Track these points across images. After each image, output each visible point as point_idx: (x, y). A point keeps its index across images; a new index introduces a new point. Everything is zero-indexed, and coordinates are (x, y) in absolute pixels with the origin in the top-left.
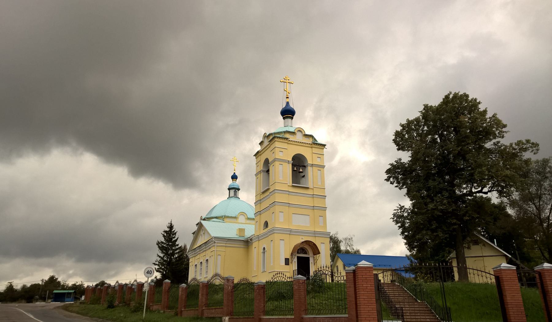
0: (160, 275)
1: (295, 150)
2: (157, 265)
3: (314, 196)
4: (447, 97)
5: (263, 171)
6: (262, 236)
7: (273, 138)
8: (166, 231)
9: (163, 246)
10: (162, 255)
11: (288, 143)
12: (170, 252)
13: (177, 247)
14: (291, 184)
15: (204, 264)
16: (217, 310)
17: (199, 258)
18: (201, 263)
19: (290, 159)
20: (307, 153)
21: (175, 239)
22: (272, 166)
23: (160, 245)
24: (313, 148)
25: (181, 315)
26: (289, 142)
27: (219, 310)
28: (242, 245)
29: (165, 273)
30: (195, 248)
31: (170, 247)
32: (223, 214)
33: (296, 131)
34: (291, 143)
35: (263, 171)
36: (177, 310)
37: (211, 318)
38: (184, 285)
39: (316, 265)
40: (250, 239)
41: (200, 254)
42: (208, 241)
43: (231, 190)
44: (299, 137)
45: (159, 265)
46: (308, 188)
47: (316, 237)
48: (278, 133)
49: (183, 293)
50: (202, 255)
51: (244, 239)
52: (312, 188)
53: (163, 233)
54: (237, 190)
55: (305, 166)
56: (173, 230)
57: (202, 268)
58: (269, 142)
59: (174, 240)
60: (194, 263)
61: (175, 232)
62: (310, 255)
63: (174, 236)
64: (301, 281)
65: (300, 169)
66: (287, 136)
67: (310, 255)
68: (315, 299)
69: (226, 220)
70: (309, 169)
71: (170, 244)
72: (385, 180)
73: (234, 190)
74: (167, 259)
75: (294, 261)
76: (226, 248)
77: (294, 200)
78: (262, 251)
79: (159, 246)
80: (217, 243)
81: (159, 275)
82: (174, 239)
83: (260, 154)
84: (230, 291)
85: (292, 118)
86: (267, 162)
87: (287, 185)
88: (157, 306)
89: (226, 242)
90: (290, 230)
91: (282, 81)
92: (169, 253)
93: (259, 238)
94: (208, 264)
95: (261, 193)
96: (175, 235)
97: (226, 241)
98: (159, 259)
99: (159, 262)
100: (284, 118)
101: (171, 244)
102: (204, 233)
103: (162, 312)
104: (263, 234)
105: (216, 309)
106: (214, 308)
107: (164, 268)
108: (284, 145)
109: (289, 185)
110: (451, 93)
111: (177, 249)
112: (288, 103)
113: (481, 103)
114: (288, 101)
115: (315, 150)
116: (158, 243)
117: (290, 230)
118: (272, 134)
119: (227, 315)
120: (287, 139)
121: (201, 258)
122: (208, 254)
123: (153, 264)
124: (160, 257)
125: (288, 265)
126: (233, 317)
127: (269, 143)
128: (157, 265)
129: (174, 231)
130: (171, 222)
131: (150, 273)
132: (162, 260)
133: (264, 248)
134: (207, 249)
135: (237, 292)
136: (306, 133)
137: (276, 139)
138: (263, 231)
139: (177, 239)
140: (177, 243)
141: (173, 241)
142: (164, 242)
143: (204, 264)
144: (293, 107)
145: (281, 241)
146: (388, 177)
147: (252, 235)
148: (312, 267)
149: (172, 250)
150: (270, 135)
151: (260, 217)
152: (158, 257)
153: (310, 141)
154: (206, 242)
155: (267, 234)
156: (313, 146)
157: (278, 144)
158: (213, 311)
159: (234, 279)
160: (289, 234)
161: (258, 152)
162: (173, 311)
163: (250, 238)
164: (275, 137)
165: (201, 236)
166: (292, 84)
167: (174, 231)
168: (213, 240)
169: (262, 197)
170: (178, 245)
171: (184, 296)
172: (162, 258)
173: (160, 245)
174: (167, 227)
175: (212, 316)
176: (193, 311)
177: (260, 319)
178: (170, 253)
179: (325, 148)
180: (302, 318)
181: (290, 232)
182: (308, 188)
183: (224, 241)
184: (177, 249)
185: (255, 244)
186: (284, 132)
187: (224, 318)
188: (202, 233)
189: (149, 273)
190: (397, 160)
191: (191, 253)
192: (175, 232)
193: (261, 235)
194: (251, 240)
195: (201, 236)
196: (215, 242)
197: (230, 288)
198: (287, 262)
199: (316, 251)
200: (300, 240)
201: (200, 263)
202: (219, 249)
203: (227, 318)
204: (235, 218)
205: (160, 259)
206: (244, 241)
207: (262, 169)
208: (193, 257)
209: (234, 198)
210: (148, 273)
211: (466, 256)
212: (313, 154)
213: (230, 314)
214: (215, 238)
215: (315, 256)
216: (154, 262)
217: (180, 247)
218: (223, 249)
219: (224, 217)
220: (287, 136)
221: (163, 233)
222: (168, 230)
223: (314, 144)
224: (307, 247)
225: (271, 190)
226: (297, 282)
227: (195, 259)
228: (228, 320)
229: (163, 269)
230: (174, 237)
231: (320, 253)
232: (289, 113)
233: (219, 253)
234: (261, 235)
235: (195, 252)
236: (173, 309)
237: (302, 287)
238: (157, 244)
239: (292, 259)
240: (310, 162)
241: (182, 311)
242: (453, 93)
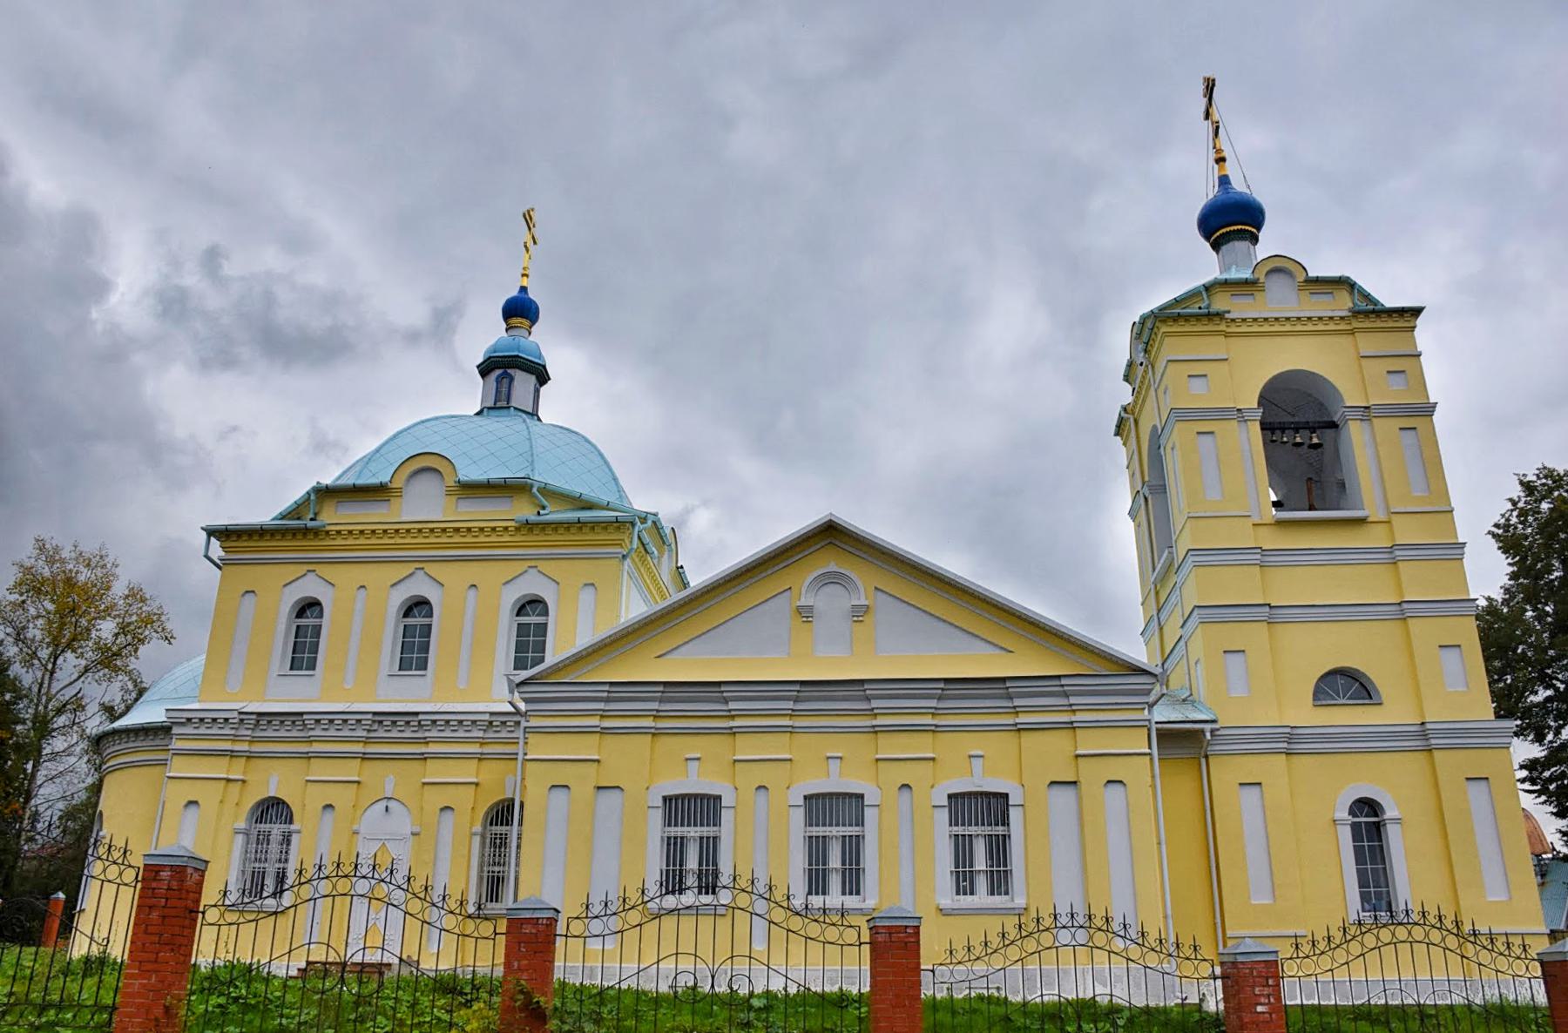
3: (1398, 553)
11: (1227, 335)
26: (1233, 329)
34: (1244, 329)
38: (244, 1030)
46: (1361, 521)
52: (1382, 517)
55: (1333, 425)
70: (1356, 435)
76: (367, 764)
87: (1250, 522)
90: (1288, 730)
100: (1216, 246)
112: (1224, 181)
115: (1370, 343)
120: (1220, 315)
135: (1374, 976)
136: (1312, 274)
144: (1248, 192)
145: (1247, 790)
153: (1342, 303)
160: (1287, 754)
182: (1361, 521)
211: (922, 967)
212: (1364, 361)
220: (1220, 303)
223: (1367, 314)
240: (1352, 397)
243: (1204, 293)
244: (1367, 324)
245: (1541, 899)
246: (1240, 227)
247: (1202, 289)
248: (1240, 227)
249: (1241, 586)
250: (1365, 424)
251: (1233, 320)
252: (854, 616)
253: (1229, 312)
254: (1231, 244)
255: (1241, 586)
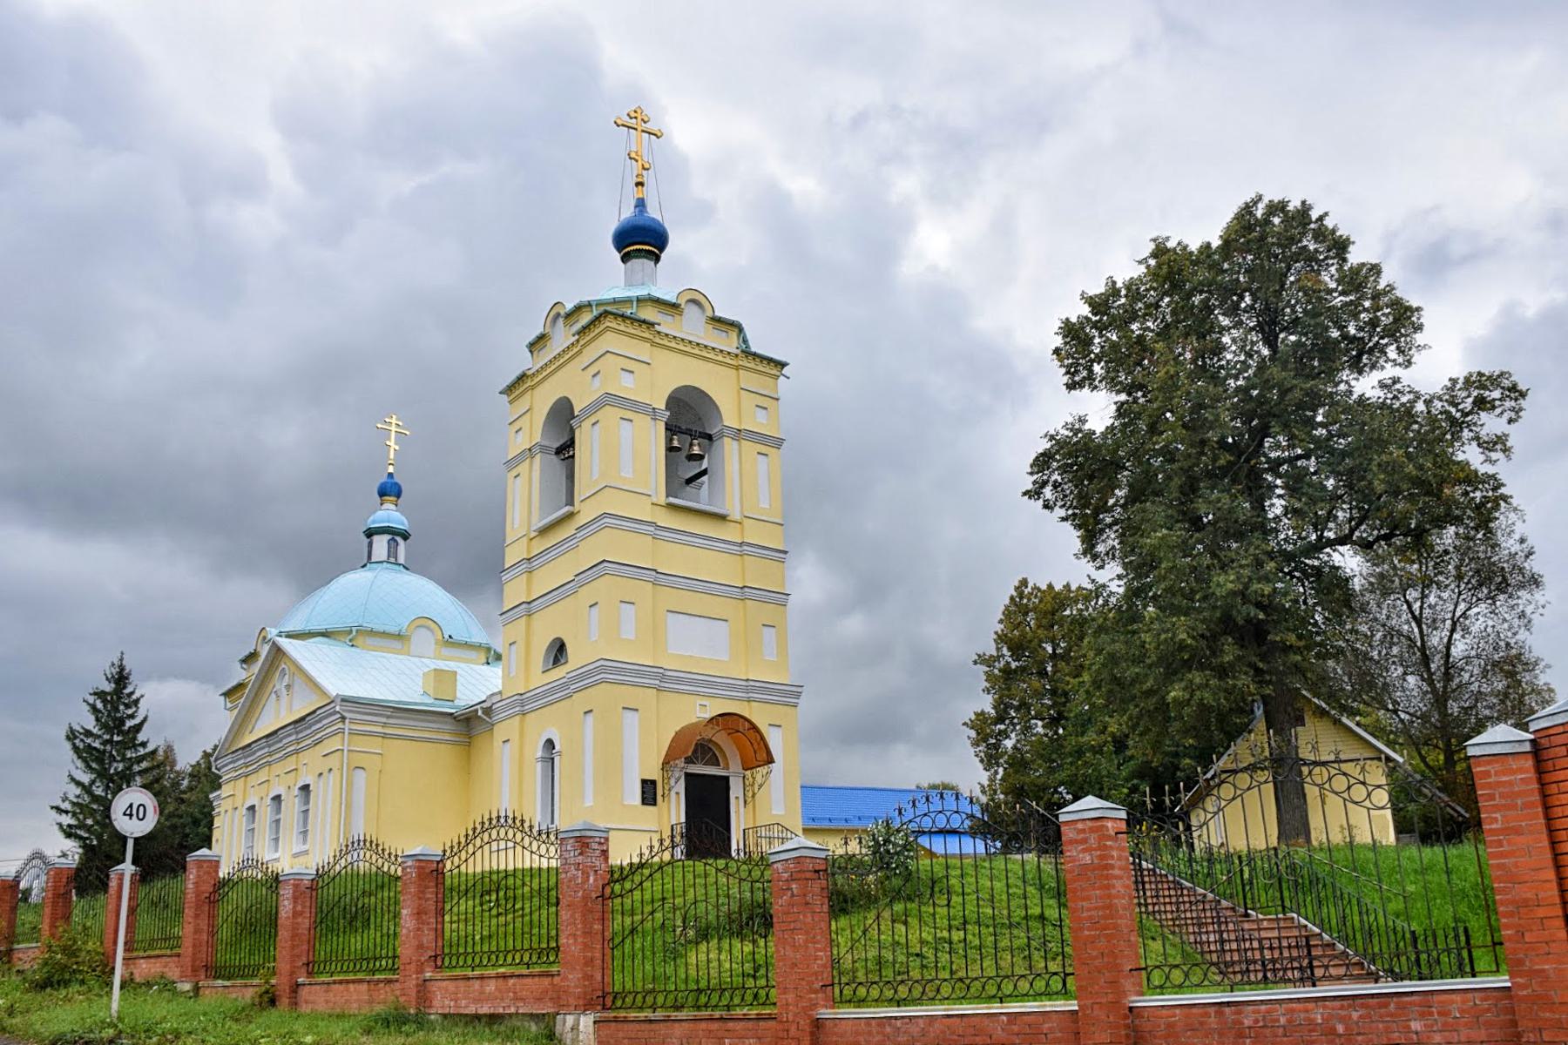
0: (80, 851)
1: (674, 372)
2: (67, 812)
3: (745, 548)
4: (1248, 209)
5: (544, 449)
6: (537, 697)
7: (597, 319)
8: (103, 692)
9: (89, 745)
10: (86, 778)
11: (653, 344)
12: (115, 769)
13: (142, 751)
14: (662, 499)
15: (292, 805)
16: (512, 981)
17: (296, 769)
18: (277, 798)
19: (661, 404)
20: (719, 385)
21: (137, 721)
22: (587, 424)
23: (77, 741)
24: (741, 371)
25: (294, 1004)
26: (657, 340)
27: (529, 980)
28: (446, 731)
29: (95, 842)
30: (249, 745)
31: (117, 751)
32: (350, 622)
33: (682, 301)
34: (665, 342)
35: (544, 449)
36: (273, 981)
37: (477, 1017)
39: (750, 806)
40: (482, 708)
41: (269, 764)
42: (314, 712)
43: (375, 538)
44: (691, 326)
45: (74, 814)
46: (722, 518)
47: (753, 704)
48: (615, 302)
49: (299, 908)
50: (279, 768)
51: (453, 711)
53: (91, 699)
54: (398, 539)
55: (710, 437)
56: (127, 691)
57: (253, 829)
58: (579, 333)
59: (130, 727)
60: (244, 799)
61: (134, 697)
62: (731, 770)
63: (130, 712)
64: (1109, 824)
65: (691, 445)
66: (648, 313)
67: (732, 770)
68: (905, 923)
69: (360, 641)
70: (729, 447)
71: (116, 738)
72: (1025, 494)
73: (389, 537)
74: (103, 794)
75: (673, 793)
76: (386, 741)
77: (675, 559)
78: (539, 754)
79: (74, 744)
80: (352, 721)
81: (74, 850)
82: (129, 723)
83: (529, 383)
84: (594, 895)
85: (657, 259)
86: (563, 415)
87: (648, 501)
88: (153, 960)
89: (384, 720)
90: (661, 671)
91: (619, 122)
92: (112, 771)
93: (523, 704)
94: (307, 802)
95: (533, 534)
96: (136, 706)
97: (388, 717)
98: (74, 791)
99: (74, 804)
100: (626, 258)
101: (120, 738)
102: (288, 687)
103: (187, 987)
104: (546, 687)
105: (504, 977)
106: (491, 972)
107: (92, 826)
108: (642, 351)
109: (655, 500)
110: (1260, 198)
111: (140, 760)
112: (641, 204)
113: (1353, 243)
114: (641, 196)
115: (750, 380)
116: (72, 736)
117: (661, 671)
118: (589, 305)
119: (587, 1007)
121: (279, 779)
122: (309, 765)
123: (52, 808)
124: (78, 783)
125: (655, 804)
126: (612, 1014)
127: (577, 337)
128: (67, 812)
129: (132, 693)
130: (121, 660)
131: (141, 816)
132: (86, 796)
133: (550, 744)
134: (274, 757)
136: (718, 314)
137: (609, 322)
138: (539, 679)
139: (145, 719)
140: (141, 737)
141: (126, 728)
142: (95, 731)
143: (292, 805)
144: (660, 219)
146: (1035, 482)
147: (493, 695)
148: (737, 812)
149: (124, 759)
150: (578, 309)
151: (528, 625)
152: (73, 786)
153: (730, 343)
154: (302, 719)
155: (565, 686)
156: (741, 363)
157: (611, 340)
158: (491, 986)
159: (607, 839)
161: (522, 378)
162: (246, 986)
163: (484, 705)
164: (606, 313)
165: (273, 696)
166: (658, 137)
167: (132, 693)
168: (338, 709)
169: (538, 546)
170: (144, 744)
171: (307, 921)
172: (87, 789)
173: (77, 741)
174: (107, 679)
175: (485, 1009)
176: (364, 987)
177: (818, 1024)
178: (117, 773)
179: (782, 377)
180: (1131, 1009)
181: (662, 680)
182: (722, 518)
183: (376, 715)
184: (140, 760)
185: (505, 729)
186: (639, 300)
187: (570, 1020)
188: (278, 683)
189: (134, 817)
190: (1070, 420)
191: (231, 763)
192: (134, 697)
193: (533, 693)
194: (488, 711)
195: (273, 696)
196: (343, 718)
197: (591, 879)
198: (649, 793)
199: (759, 755)
200: (700, 710)
201: (273, 799)
202: (361, 744)
203: (587, 1022)
204: (399, 636)
205: (78, 791)
206: (455, 718)
207: (537, 438)
208: (236, 778)
209: (389, 565)
210: (131, 815)
212: (742, 392)
213: (603, 1000)
214: (343, 700)
215: (748, 773)
216: (1029, 470)
217: (154, 752)
218: (374, 745)
219: (357, 631)
221: (91, 699)
222: (108, 687)
224: (721, 739)
225: (582, 520)
226: (1092, 830)
227: (250, 785)
228: (591, 1029)
229: (88, 829)
230: (132, 716)
231: (770, 760)
232: (647, 240)
233: (359, 760)
234: (533, 693)
235: (245, 757)
236: (253, 976)
237: (1115, 853)
238: (68, 738)
239: (668, 783)
240: (729, 419)
241: (295, 988)
242: (1266, 200)
243: (635, 303)
244: (752, 365)
245: (662, 769)
246: (651, 248)
247: (635, 299)
248: (651, 248)
249: (636, 550)
250: (735, 443)
251: (659, 333)
252: (1240, 857)
253: (659, 324)
254: (641, 260)
255: (636, 550)
